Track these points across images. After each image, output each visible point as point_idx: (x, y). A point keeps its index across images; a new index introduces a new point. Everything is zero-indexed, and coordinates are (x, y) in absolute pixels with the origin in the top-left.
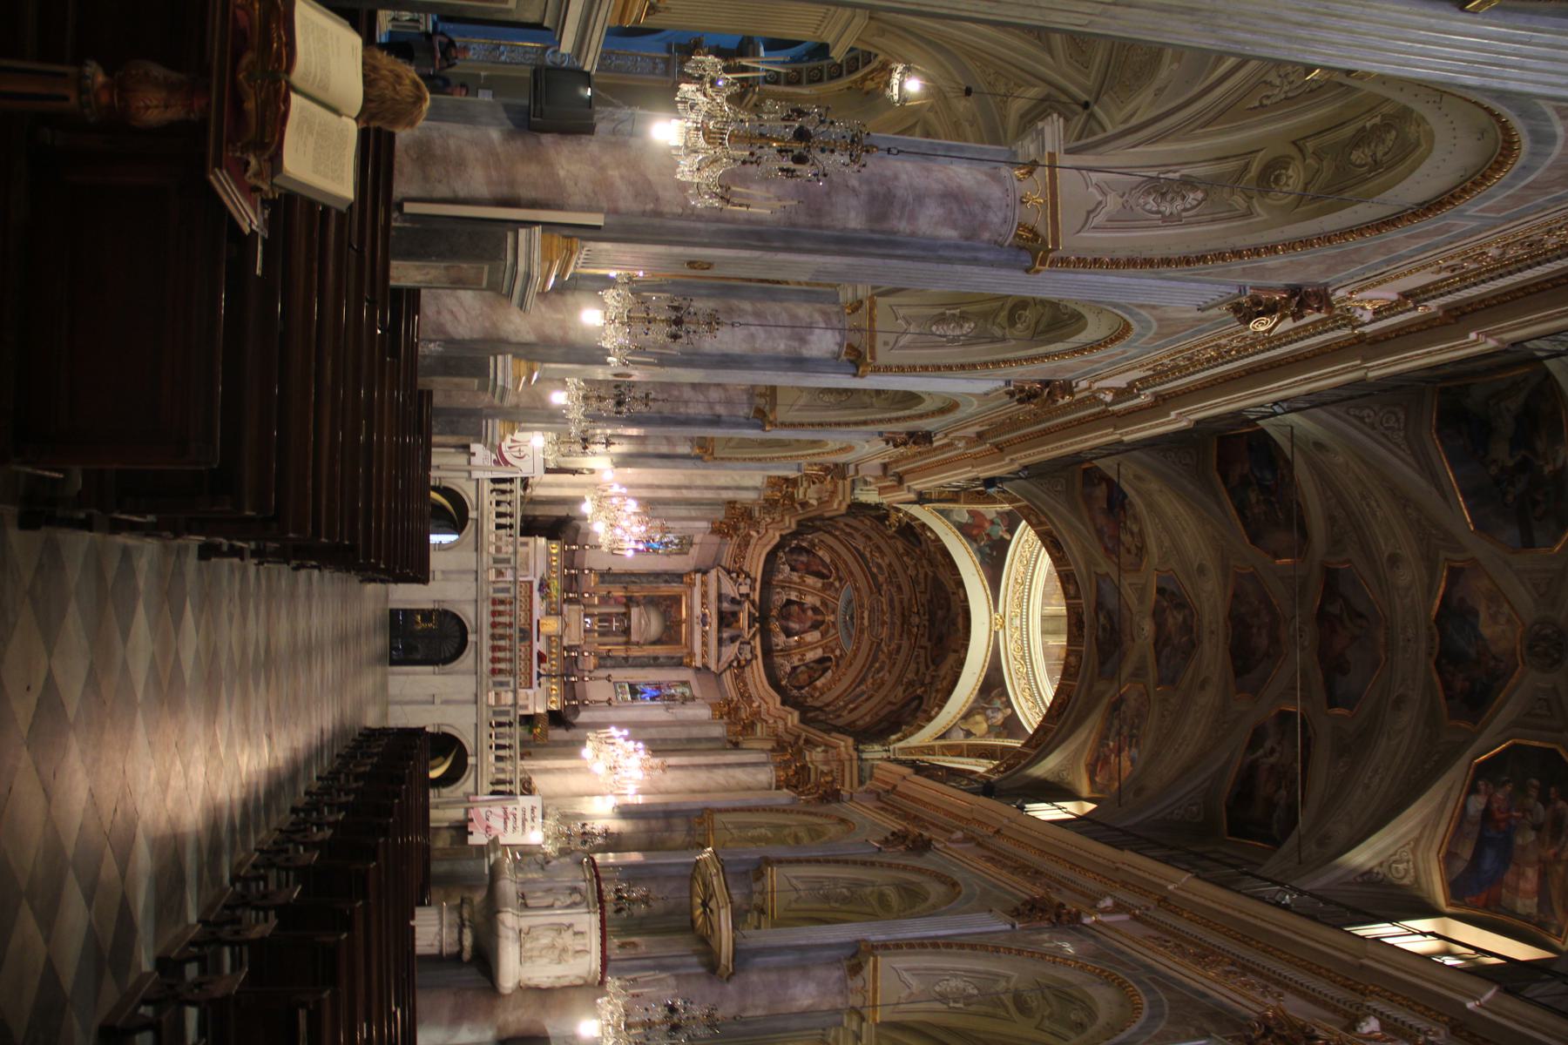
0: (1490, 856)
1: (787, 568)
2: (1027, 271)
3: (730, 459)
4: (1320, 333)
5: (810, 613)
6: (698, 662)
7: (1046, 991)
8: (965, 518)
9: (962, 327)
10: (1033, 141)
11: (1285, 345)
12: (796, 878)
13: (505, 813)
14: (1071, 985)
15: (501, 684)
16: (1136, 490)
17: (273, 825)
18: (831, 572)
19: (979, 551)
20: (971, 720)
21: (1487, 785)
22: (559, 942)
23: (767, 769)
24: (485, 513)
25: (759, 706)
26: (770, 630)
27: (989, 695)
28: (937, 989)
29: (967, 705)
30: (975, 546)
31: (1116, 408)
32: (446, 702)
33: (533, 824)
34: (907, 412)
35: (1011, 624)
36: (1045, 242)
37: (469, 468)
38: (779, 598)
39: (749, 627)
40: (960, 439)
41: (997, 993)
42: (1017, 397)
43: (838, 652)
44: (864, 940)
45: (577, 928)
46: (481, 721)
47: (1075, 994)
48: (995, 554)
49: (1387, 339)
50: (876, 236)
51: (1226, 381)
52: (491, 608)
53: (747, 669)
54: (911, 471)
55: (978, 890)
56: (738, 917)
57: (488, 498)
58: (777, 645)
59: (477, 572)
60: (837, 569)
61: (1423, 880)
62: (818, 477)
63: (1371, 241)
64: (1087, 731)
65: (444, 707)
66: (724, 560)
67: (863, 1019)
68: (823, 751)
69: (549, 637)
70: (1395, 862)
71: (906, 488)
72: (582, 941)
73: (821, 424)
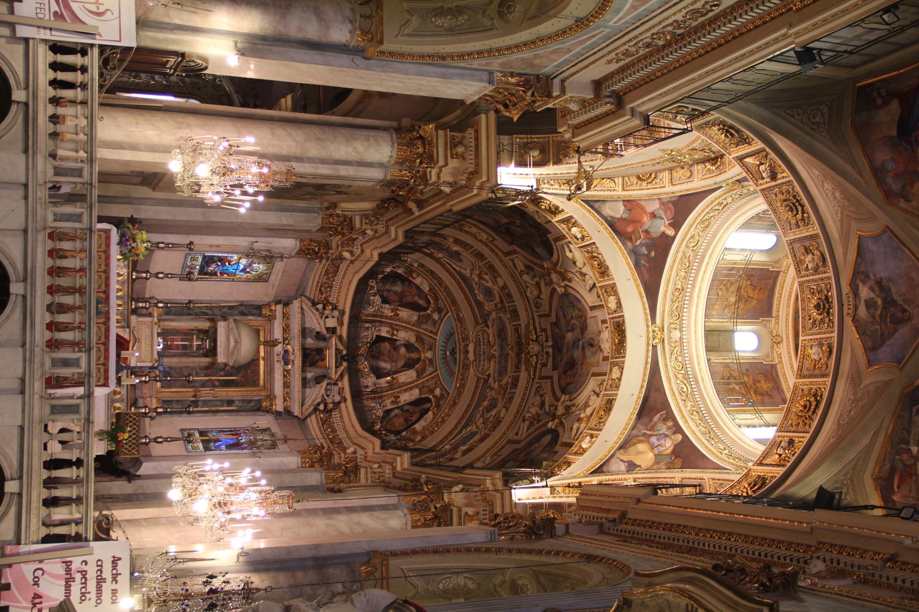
1: (377, 299)
5: (403, 350)
6: (279, 406)
13: (68, 571)
18: (429, 303)
19: (634, 253)
20: (632, 450)
23: (399, 513)
25: (355, 452)
26: (358, 371)
30: (629, 244)
33: (114, 586)
37: (10, 19)
38: (368, 334)
39: (337, 367)
43: (438, 392)
46: (31, 422)
48: (653, 254)
53: (335, 414)
58: (367, 387)
59: (26, 186)
60: (436, 298)
66: (308, 290)
68: (462, 490)
71: (628, 112)
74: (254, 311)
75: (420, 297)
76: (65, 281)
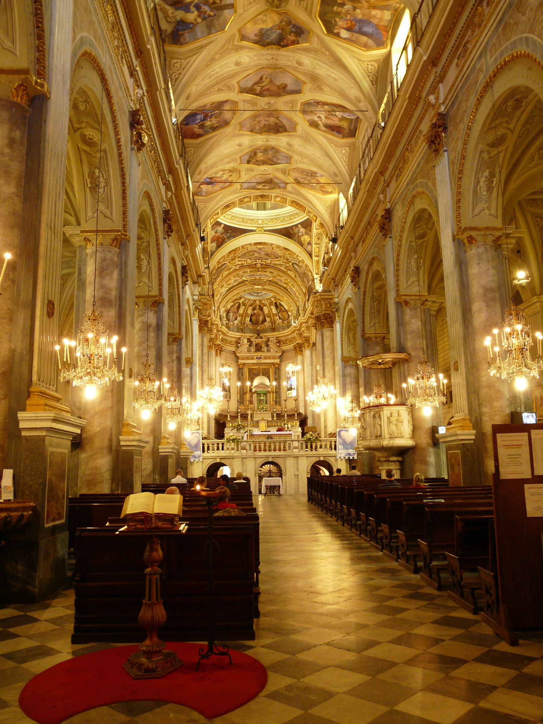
0: (368, 29)
2: (129, 241)
3: (192, 351)
4: (146, 109)
5: (255, 311)
7: (416, 226)
8: (214, 245)
9: (143, 259)
10: (74, 238)
11: (150, 123)
14: (414, 217)
15: (290, 447)
16: (205, 174)
17: (349, 531)
19: (229, 238)
22: (394, 422)
23: (324, 332)
24: (217, 455)
28: (415, 270)
31: (173, 189)
32: (298, 469)
34: (175, 278)
35: (261, 224)
36: (119, 235)
40: (184, 253)
41: (417, 246)
42: (170, 233)
44: (395, 299)
45: (389, 415)
47: (417, 215)
49: (149, 81)
50: (117, 304)
51: (164, 145)
52: (258, 451)
53: (280, 339)
54: (196, 272)
55: (376, 249)
56: (387, 350)
57: (211, 454)
61: (376, 58)
62: (199, 312)
63: (115, 100)
65: (300, 471)
67: (426, 300)
69: (268, 426)
70: (368, 70)
73: (179, 314)
76: (262, 447)
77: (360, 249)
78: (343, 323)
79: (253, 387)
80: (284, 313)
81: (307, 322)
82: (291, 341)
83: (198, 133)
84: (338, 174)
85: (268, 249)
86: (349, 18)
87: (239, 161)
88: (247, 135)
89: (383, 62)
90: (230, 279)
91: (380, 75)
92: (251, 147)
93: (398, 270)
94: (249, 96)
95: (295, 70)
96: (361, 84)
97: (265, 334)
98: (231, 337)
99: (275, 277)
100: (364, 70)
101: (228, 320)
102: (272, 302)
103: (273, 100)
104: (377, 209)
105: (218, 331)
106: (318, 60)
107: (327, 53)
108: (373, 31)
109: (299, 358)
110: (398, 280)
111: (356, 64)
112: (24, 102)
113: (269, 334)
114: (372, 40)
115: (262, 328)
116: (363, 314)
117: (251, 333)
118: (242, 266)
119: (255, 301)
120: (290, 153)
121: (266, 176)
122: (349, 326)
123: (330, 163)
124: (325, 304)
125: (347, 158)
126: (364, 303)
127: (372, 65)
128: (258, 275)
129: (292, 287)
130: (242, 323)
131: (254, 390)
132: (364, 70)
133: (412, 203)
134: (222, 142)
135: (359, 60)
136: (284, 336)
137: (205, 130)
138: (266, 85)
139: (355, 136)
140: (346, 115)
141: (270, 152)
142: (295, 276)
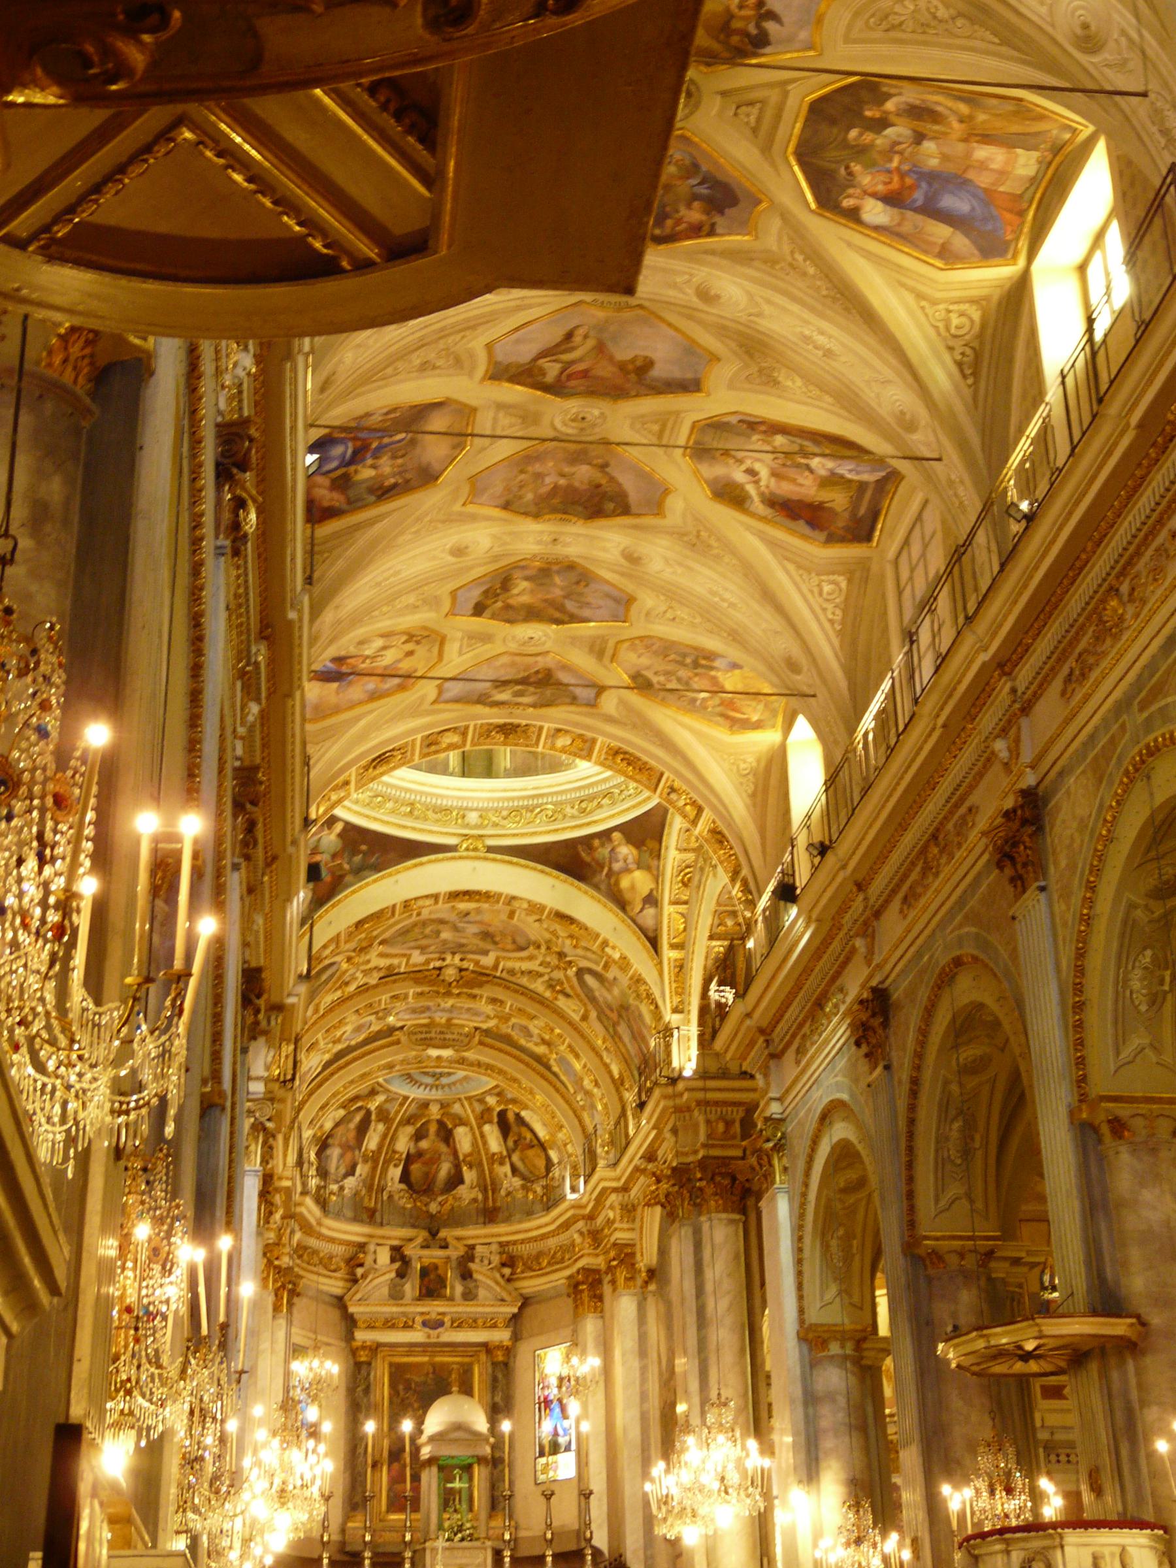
0: (950, 202)
5: (424, 1144)
12: (937, 1200)
18: (360, 1108)
19: (360, 872)
20: (628, 896)
21: (849, 196)
23: (706, 1227)
27: (588, 865)
28: (1143, 1008)
29: (603, 899)
30: (348, 878)
35: (477, 827)
44: (1071, 1113)
48: (364, 847)
64: (679, 729)
70: (948, 329)
72: (1108, 1559)
74: (364, 1372)
75: (350, 1121)
77: (892, 925)
78: (804, 1195)
79: (424, 1438)
80: (530, 1153)
81: (625, 1189)
82: (557, 1259)
83: (326, 504)
84: (804, 662)
85: (493, 916)
86: (895, 164)
87: (447, 605)
88: (488, 518)
89: (1000, 304)
90: (341, 1023)
91: (988, 347)
92: (496, 558)
93: (1079, 1007)
94: (517, 393)
95: (690, 317)
96: (922, 372)
97: (459, 1232)
98: (332, 1240)
99: (505, 1019)
100: (936, 328)
101: (323, 1173)
102: (489, 1110)
103: (594, 409)
104: (972, 788)
105: (289, 1216)
106: (776, 289)
107: (811, 270)
108: (973, 209)
109: (590, 1326)
110: (1080, 1043)
111: (911, 313)
112: (81, 380)
113: (474, 1233)
114: (967, 235)
115: (447, 1207)
116: (910, 1165)
117: (403, 1225)
118: (390, 975)
119: (425, 1105)
120: (629, 587)
121: (531, 660)
122: (828, 1207)
123: (776, 623)
124: (708, 1122)
125: (838, 612)
126: (912, 1122)
127: (962, 314)
128: (443, 1009)
129: (571, 1058)
130: (373, 1185)
131: (426, 1452)
132: (936, 328)
133: (1141, 769)
134: (401, 540)
135: (920, 296)
136: (530, 1240)
137: (351, 493)
138: (581, 360)
139: (869, 538)
140: (846, 469)
141: (557, 580)
142: (585, 1018)
